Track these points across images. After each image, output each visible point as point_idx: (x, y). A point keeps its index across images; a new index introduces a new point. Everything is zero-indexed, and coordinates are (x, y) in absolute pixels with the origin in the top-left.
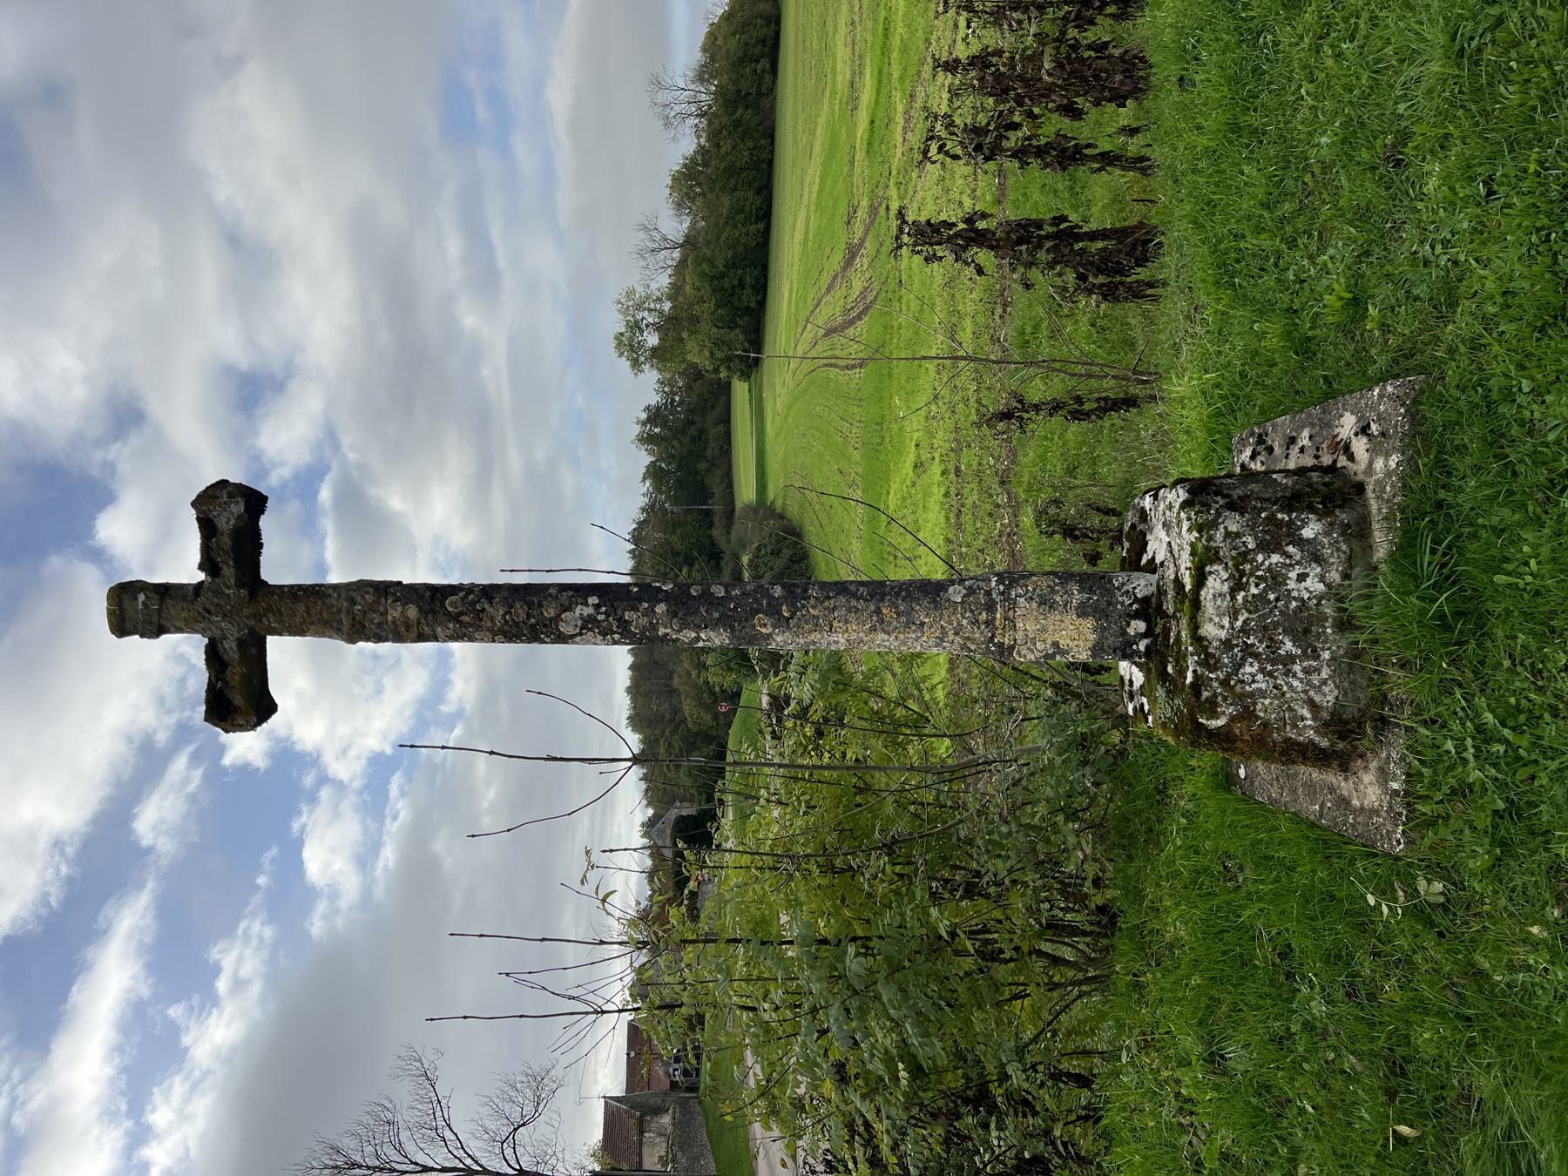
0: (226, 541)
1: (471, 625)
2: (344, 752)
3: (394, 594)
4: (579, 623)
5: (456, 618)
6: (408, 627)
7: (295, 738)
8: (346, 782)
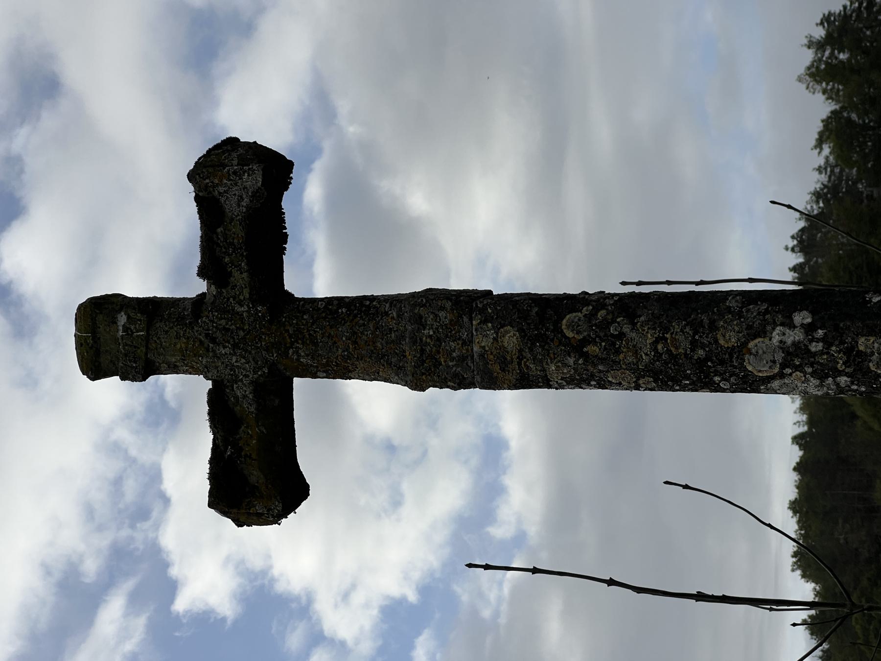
0: (237, 231)
1: (602, 360)
2: (346, 596)
3: (482, 311)
4: (779, 356)
5: (578, 348)
6: (504, 364)
7: (276, 572)
8: (350, 643)
